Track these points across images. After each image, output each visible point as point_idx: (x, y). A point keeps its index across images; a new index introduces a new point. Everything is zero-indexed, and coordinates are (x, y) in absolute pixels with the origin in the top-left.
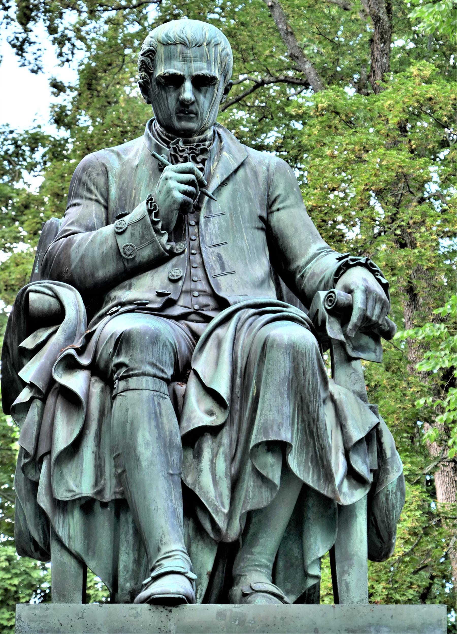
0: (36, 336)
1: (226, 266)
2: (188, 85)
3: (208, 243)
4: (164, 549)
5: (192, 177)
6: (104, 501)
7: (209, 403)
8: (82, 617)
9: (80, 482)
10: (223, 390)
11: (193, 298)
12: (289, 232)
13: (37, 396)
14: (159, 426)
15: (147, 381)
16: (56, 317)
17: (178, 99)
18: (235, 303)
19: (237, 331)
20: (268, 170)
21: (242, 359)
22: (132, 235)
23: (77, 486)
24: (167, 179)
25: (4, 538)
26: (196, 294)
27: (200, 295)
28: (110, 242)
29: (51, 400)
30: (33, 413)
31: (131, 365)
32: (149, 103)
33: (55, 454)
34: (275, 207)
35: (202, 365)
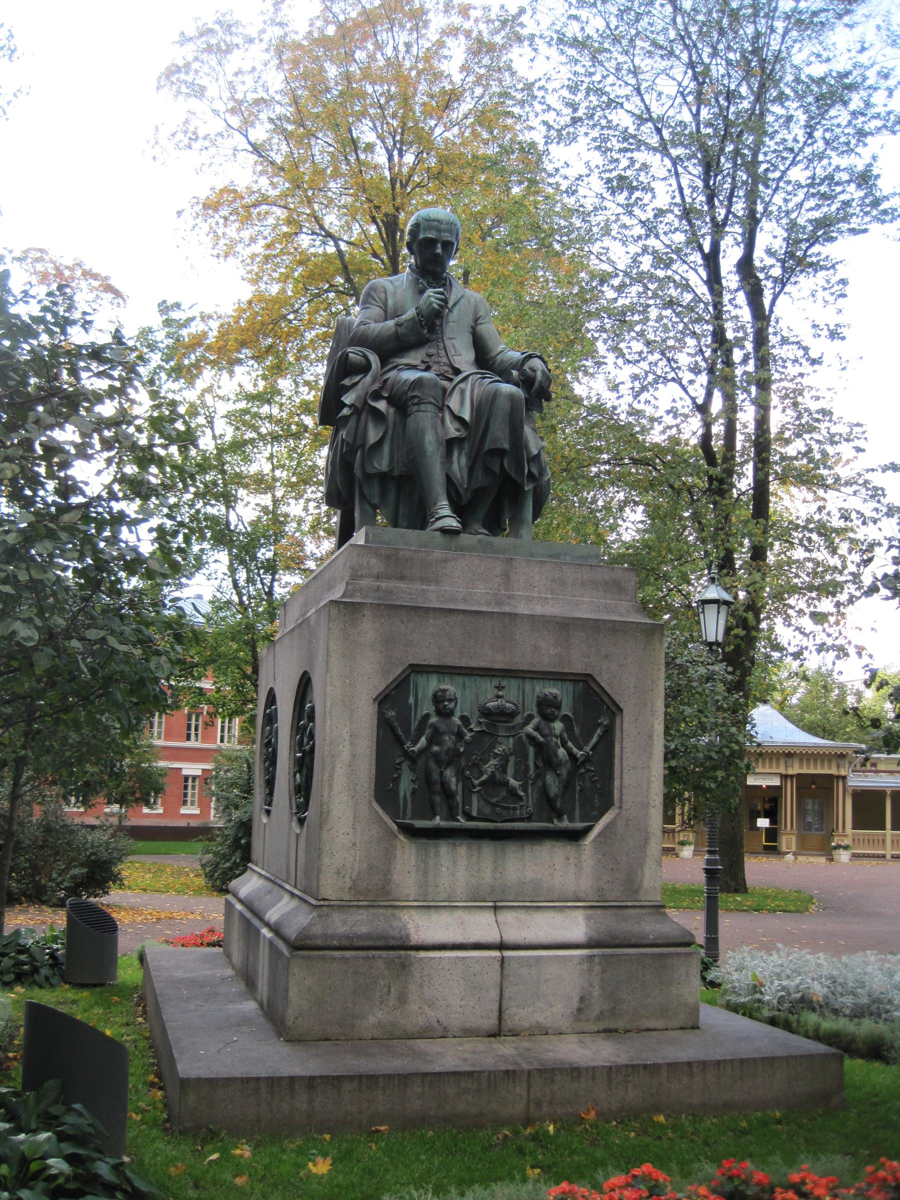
10: (467, 416)
12: (486, 336)
14: (436, 433)
16: (365, 368)
19: (473, 386)
25: (897, 1014)
28: (393, 329)
29: (363, 416)
30: (352, 422)
33: (367, 447)
35: (453, 402)
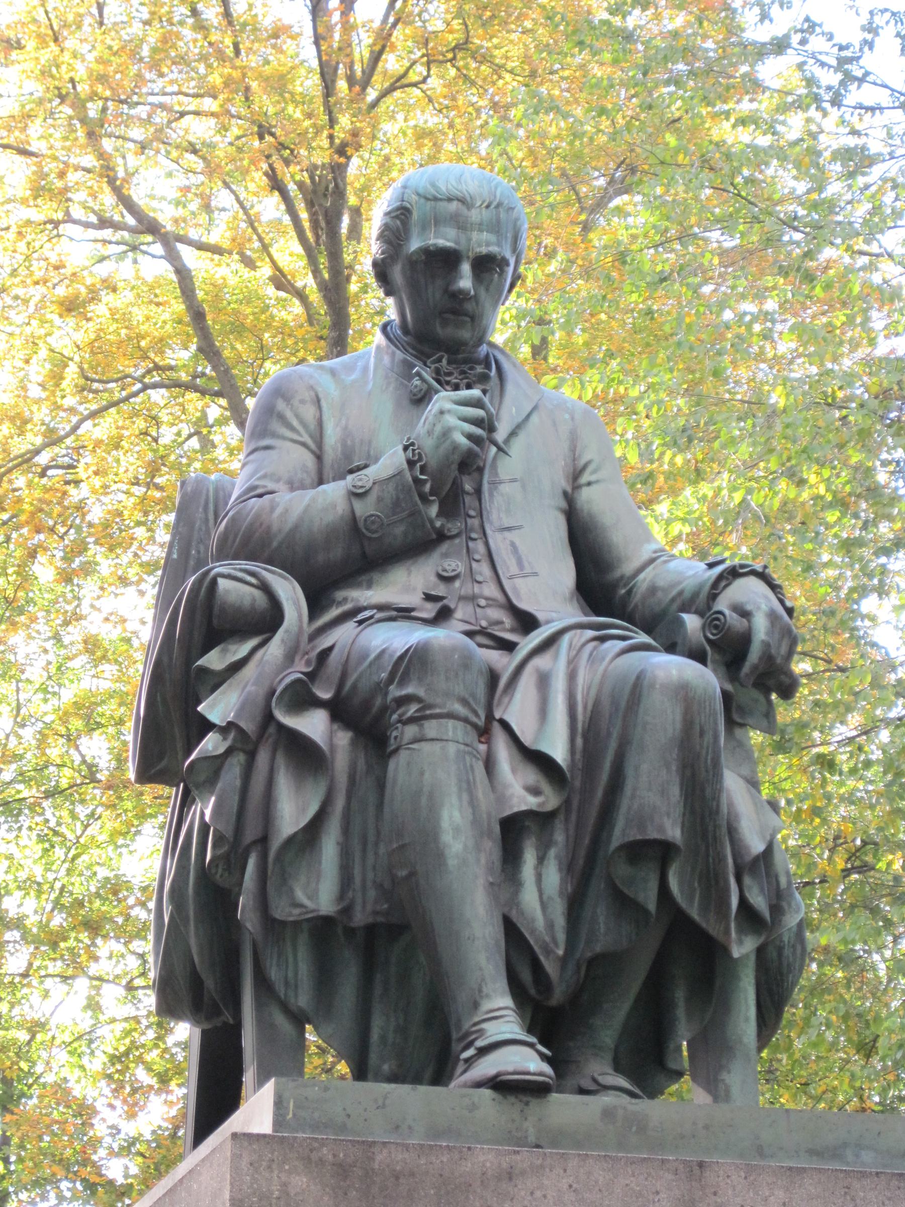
0: (224, 651)
1: (526, 564)
2: (466, 268)
3: (497, 524)
4: (487, 1005)
5: (480, 413)
6: (352, 925)
7: (531, 775)
8: (384, 1106)
9: (317, 891)
10: (559, 752)
11: (478, 610)
13: (239, 745)
14: (473, 803)
15: (455, 728)
16: (268, 620)
17: (446, 291)
18: (548, 622)
20: (573, 419)
21: (585, 707)
22: (380, 500)
23: (309, 898)
24: (442, 412)
26: (483, 602)
27: (488, 606)
28: (341, 507)
30: (232, 774)
31: (429, 699)
32: (388, 294)
34: (584, 479)
